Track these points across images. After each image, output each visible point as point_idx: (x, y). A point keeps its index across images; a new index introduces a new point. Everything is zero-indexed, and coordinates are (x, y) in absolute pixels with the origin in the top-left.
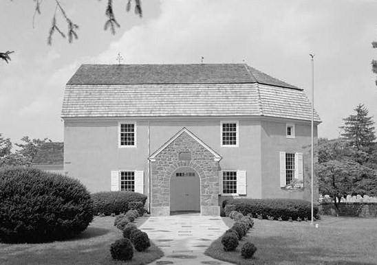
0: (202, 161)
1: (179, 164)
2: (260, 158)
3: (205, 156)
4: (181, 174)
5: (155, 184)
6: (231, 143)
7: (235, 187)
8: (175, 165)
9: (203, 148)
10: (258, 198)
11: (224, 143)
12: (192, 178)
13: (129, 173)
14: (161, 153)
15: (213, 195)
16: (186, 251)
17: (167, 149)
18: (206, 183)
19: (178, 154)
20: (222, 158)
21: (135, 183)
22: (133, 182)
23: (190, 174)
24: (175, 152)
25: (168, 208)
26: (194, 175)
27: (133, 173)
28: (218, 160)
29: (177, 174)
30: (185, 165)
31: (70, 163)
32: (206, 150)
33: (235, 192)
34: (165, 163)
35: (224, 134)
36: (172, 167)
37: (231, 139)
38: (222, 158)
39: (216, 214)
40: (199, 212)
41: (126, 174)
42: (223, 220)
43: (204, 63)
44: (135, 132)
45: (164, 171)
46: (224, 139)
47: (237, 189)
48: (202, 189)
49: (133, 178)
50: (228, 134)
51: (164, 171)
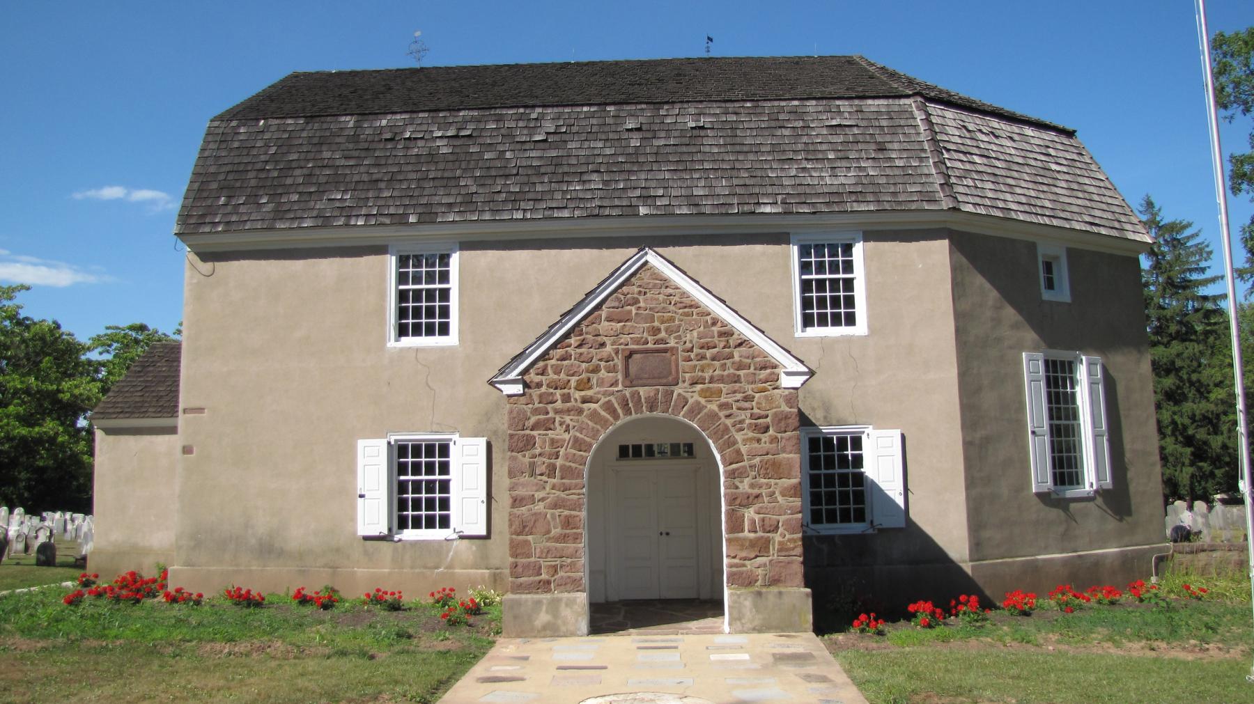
0: (725, 388)
1: (625, 405)
2: (953, 373)
3: (740, 366)
4: (650, 448)
5: (521, 492)
6: (836, 321)
7: (445, 504)
8: (609, 407)
9: (727, 333)
10: (449, 693)
11: (807, 321)
12: (681, 465)
13: (430, 450)
14: (544, 356)
15: (777, 537)
16: (1105, 511)
17: (573, 340)
18: (745, 486)
19: (619, 362)
20: (812, 373)
21: (453, 487)
22: (445, 486)
23: (675, 450)
24: (609, 349)
25: (582, 598)
26: (690, 449)
27: (444, 450)
28: (797, 382)
29: (624, 452)
30: (652, 407)
31: (200, 410)
32: (742, 343)
33: (445, 522)
34: (567, 398)
35: (806, 285)
36: (594, 416)
37: (835, 302)
38: (812, 373)
39: (796, 628)
40: (713, 606)
41: (417, 451)
42: (835, 649)
43: (712, 54)
44: (454, 284)
45: (558, 433)
46: (806, 303)
47: (454, 513)
48: (731, 514)
49: (445, 468)
50: (821, 284)
51: (558, 433)
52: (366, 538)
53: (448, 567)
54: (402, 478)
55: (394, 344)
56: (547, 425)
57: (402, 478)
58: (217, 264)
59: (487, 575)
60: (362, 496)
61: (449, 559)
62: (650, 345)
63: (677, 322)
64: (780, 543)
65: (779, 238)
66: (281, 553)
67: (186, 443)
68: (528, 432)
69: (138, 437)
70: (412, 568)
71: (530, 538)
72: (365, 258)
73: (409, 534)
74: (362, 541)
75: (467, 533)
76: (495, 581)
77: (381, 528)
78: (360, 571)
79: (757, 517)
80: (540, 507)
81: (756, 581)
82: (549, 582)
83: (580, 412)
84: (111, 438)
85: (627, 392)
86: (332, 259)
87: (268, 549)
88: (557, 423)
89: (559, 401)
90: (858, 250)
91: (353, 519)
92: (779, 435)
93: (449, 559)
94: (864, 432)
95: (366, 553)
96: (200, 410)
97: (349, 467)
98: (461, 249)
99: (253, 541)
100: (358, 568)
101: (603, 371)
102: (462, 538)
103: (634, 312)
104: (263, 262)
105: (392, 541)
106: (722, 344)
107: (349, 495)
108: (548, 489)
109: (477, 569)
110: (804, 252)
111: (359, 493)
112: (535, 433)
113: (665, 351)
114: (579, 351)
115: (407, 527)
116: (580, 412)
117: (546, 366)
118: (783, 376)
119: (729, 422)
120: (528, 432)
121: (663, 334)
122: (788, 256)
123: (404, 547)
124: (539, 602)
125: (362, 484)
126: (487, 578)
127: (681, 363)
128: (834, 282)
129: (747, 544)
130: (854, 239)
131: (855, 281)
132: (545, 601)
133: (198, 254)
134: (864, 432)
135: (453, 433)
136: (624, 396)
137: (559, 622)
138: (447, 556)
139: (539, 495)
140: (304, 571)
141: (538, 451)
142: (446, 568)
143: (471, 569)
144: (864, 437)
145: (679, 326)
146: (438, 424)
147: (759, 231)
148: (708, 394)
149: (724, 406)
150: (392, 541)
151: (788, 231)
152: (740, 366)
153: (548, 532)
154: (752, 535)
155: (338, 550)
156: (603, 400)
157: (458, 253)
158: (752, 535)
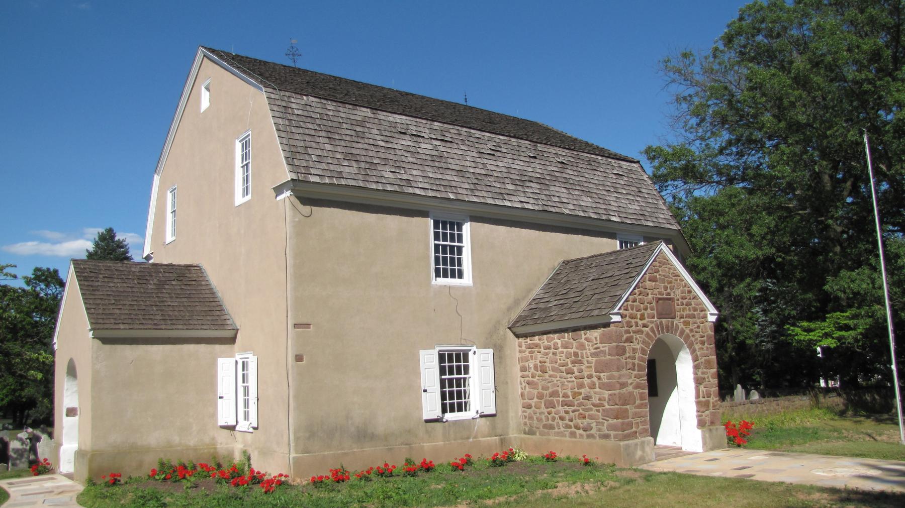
11: (438, 275)
24: (650, 296)
52: (427, 421)
53: (475, 437)
54: (443, 377)
55: (467, 280)
56: (629, 340)
57: (443, 377)
58: (314, 208)
59: (497, 440)
60: (425, 391)
61: (475, 432)
62: (664, 296)
63: (673, 284)
64: (713, 403)
65: (424, 214)
66: (373, 437)
67: (298, 353)
68: (623, 344)
69: (134, 346)
70: (455, 440)
71: (628, 407)
72: (416, 218)
73: (449, 416)
74: (424, 423)
75: (486, 413)
76: (502, 443)
77: (437, 412)
78: (427, 445)
79: (705, 390)
80: (630, 388)
81: (706, 423)
82: (636, 432)
83: (642, 332)
84: (108, 347)
85: (658, 322)
86: (382, 215)
87: (364, 435)
88: (634, 339)
89: (634, 326)
90: (467, 228)
91: (420, 408)
92: (709, 346)
93: (475, 432)
94: (470, 350)
95: (427, 432)
96: (308, 325)
97: (415, 370)
98: (471, 221)
99: (353, 429)
100: (423, 443)
101: (649, 309)
102: (481, 416)
103: (658, 277)
104: (347, 212)
105: (443, 422)
106: (688, 298)
107: (415, 390)
108: (633, 377)
109: (490, 437)
110: (436, 226)
111: (219, 396)
112: (626, 344)
113: (669, 299)
114: (640, 297)
115: (447, 412)
116: (642, 332)
117: (627, 305)
118: (709, 315)
119: (693, 339)
120: (623, 344)
121: (669, 290)
122: (427, 225)
123: (449, 425)
124: (636, 445)
125: (221, 391)
126: (497, 443)
127: (676, 307)
128: (452, 247)
129: (703, 404)
130: (464, 220)
131: (463, 249)
132: (639, 443)
133: (299, 198)
134: (470, 350)
135: (472, 345)
136: (657, 324)
137: (645, 455)
138: (474, 429)
139: (630, 381)
140: (391, 449)
141: (628, 355)
142: (473, 438)
143: (487, 437)
144: (471, 354)
145: (674, 286)
146: (465, 339)
147: (591, 229)
148: (686, 324)
149: (691, 330)
150: (443, 422)
151: (617, 232)
152: (695, 310)
153: (635, 403)
154: (703, 399)
155: (409, 431)
156: (651, 326)
157: (469, 223)
158: (703, 399)
